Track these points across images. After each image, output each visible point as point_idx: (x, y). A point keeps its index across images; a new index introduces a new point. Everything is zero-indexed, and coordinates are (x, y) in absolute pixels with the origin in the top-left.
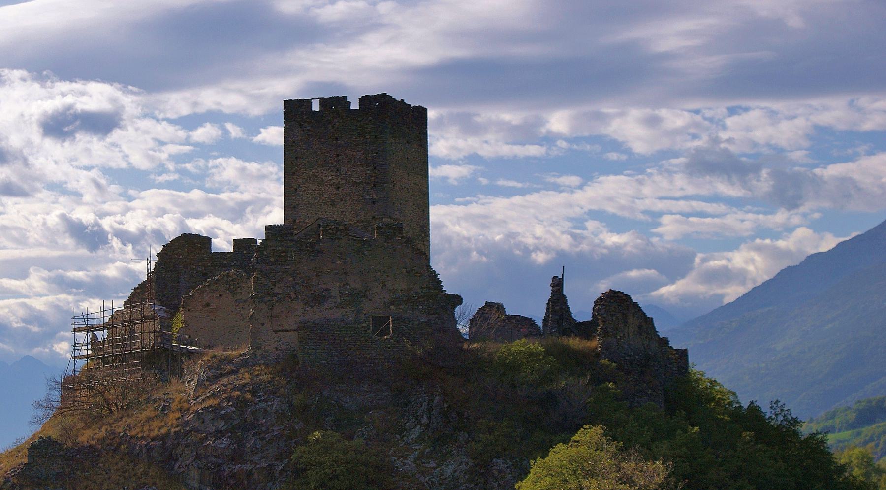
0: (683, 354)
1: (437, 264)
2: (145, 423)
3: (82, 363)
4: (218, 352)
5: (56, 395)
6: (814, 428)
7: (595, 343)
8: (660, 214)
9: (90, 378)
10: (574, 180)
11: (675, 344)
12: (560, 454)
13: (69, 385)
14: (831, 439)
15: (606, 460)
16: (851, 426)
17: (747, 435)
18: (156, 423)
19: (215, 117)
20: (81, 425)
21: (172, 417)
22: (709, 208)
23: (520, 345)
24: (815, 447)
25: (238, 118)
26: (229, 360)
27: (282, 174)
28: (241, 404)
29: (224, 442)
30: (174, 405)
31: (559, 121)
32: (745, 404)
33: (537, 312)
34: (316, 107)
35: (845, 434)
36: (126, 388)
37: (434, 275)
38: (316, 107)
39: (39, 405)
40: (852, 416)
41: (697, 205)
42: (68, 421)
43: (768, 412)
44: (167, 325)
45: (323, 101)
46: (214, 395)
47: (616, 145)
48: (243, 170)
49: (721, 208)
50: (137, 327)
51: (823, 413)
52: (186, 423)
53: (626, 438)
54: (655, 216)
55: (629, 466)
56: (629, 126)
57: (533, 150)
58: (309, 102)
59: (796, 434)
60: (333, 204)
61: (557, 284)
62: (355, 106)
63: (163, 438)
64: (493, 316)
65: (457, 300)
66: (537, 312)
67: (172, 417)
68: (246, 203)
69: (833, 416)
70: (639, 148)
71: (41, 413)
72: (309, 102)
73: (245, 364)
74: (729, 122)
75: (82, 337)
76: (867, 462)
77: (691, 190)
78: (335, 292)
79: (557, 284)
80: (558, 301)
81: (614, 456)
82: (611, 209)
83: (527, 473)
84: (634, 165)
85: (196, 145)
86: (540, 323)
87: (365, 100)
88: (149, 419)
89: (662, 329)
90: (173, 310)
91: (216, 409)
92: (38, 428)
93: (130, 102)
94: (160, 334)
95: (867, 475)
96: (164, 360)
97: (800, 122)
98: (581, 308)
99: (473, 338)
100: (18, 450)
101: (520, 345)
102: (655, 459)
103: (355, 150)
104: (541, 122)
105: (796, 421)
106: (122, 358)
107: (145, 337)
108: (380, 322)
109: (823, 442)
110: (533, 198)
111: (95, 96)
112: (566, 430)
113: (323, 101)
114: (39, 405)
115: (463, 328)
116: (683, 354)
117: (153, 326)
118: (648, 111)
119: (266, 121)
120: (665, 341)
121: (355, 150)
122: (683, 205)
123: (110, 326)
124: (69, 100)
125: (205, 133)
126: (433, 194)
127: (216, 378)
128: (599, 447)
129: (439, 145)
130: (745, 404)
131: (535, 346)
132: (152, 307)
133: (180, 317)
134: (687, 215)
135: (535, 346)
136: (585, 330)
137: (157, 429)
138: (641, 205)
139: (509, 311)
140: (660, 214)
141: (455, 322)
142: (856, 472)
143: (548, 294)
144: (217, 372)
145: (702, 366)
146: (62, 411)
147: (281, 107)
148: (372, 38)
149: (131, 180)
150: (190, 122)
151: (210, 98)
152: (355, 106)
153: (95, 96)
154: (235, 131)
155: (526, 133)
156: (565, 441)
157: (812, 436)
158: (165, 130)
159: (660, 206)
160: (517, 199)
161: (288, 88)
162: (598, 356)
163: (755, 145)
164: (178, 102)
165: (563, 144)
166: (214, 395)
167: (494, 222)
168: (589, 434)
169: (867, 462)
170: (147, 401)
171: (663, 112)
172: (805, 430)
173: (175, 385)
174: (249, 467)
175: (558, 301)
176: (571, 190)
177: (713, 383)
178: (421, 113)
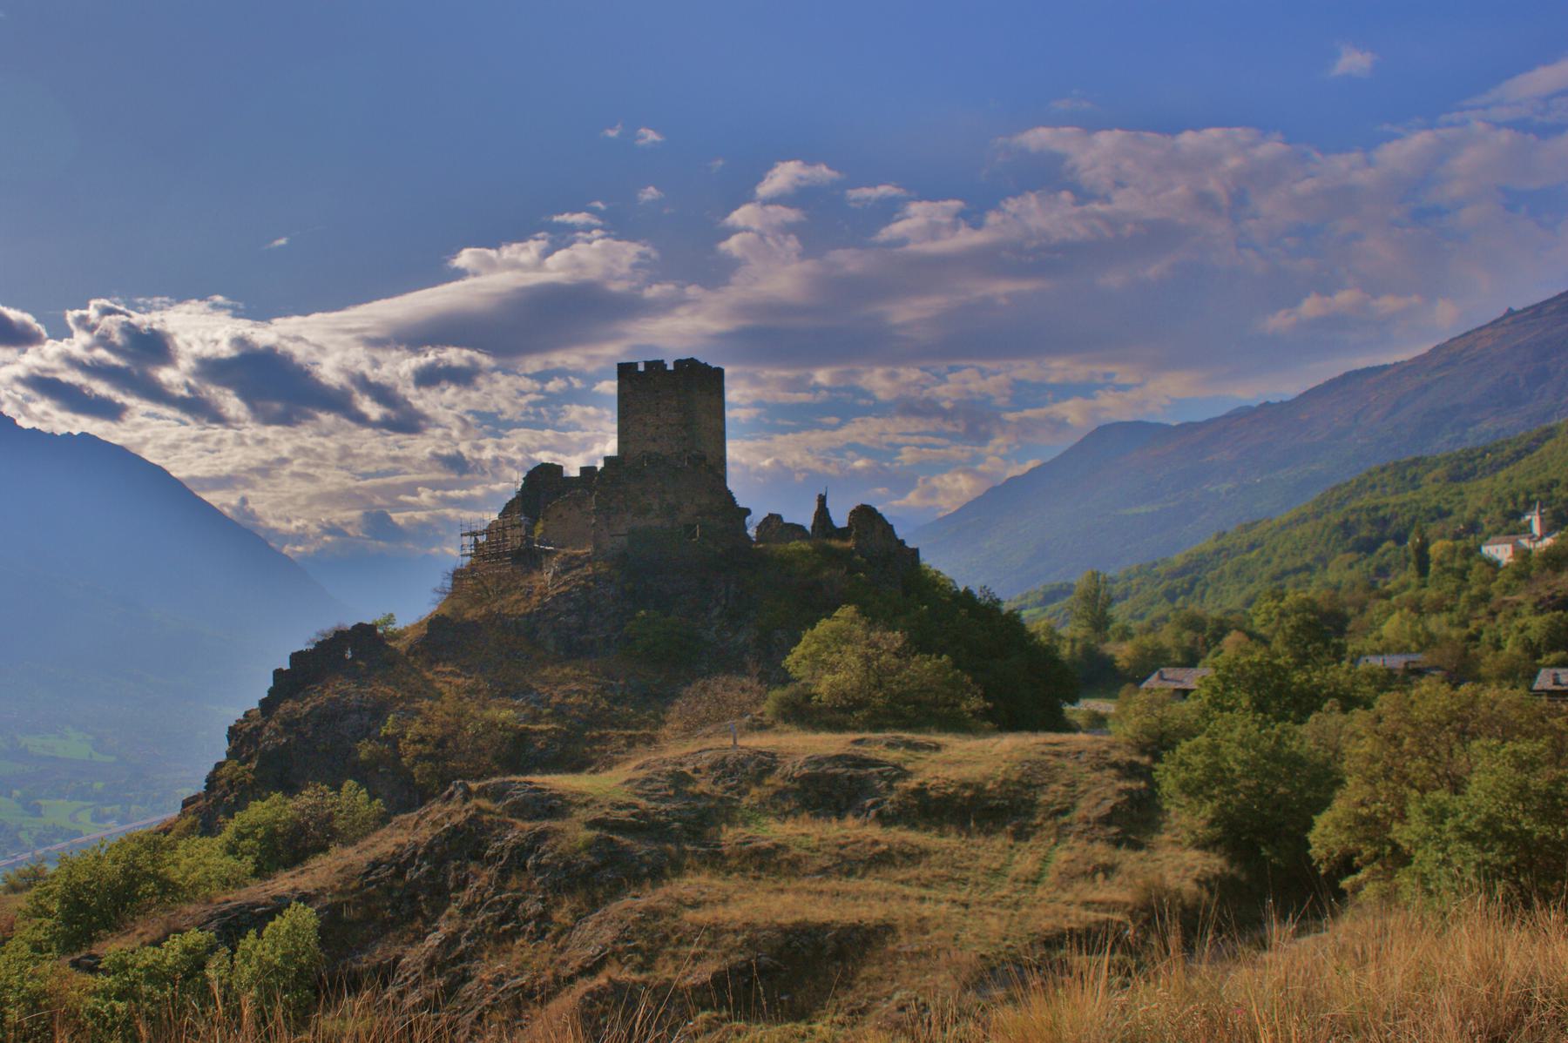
0: (916, 552)
1: (734, 483)
2: (513, 605)
3: (467, 560)
4: (568, 551)
5: (448, 583)
6: (1012, 606)
7: (850, 544)
8: (901, 446)
9: (473, 571)
10: (834, 420)
11: (910, 544)
12: (824, 627)
13: (458, 575)
14: (1025, 614)
15: (859, 631)
16: (1039, 605)
17: (963, 612)
18: (523, 604)
19: (562, 373)
20: (466, 606)
21: (535, 599)
22: (938, 441)
23: (794, 545)
24: (1013, 620)
25: (578, 373)
26: (576, 557)
27: (616, 416)
28: (586, 588)
29: (573, 619)
30: (536, 591)
31: (822, 376)
32: (962, 589)
33: (806, 520)
34: (641, 368)
35: (1035, 611)
36: (500, 578)
37: (729, 493)
38: (641, 368)
39: (435, 591)
40: (1040, 598)
41: (930, 440)
42: (457, 603)
43: (978, 595)
44: (530, 531)
45: (647, 364)
46: (566, 583)
47: (866, 394)
48: (585, 414)
49: (947, 442)
50: (508, 533)
51: (1018, 596)
52: (545, 605)
53: (872, 615)
54: (896, 448)
55: (875, 635)
56: (876, 381)
57: (802, 397)
58: (636, 364)
59: (999, 611)
60: (654, 440)
61: (822, 500)
62: (670, 367)
63: (529, 615)
64: (774, 524)
65: (747, 512)
66: (806, 520)
67: (535, 599)
68: (592, 441)
69: (1026, 597)
70: (881, 395)
71: (437, 596)
72: (636, 364)
73: (589, 560)
74: (950, 377)
75: (468, 540)
76: (1051, 631)
77: (922, 428)
78: (656, 507)
79: (822, 500)
80: (822, 514)
81: (864, 628)
82: (862, 441)
83: (799, 640)
84: (881, 410)
85: (549, 394)
86: (809, 529)
87: (678, 363)
88: (517, 601)
89: (900, 533)
90: (535, 520)
91: (567, 594)
92: (434, 608)
93: (485, 361)
94: (524, 538)
95: (1051, 640)
96: (528, 558)
97: (1002, 377)
98: (840, 518)
99: (759, 540)
100: (421, 624)
101: (794, 545)
102: (894, 630)
103: (672, 402)
104: (811, 376)
105: (999, 601)
106: (498, 556)
107: (514, 540)
108: (690, 529)
109: (1018, 616)
110: (803, 435)
111: (454, 356)
112: (828, 609)
113: (647, 364)
114: (435, 591)
115: (752, 532)
116: (916, 552)
117: (520, 531)
118: (889, 369)
119: (600, 376)
120: (902, 542)
121: (672, 402)
122: (916, 439)
123: (488, 532)
124: (248, 331)
125: (553, 386)
126: (729, 431)
127: (566, 571)
128: (853, 621)
129: (732, 394)
130: (962, 589)
131: (805, 546)
132: (519, 518)
133: (540, 525)
134: (920, 446)
135: (805, 546)
136: (843, 534)
137: (523, 609)
138: (885, 439)
139: (786, 520)
140: (901, 446)
141: (745, 528)
142: (1043, 638)
143: (814, 507)
144: (568, 565)
145: (928, 560)
146: (453, 594)
147: (616, 369)
148: (681, 311)
149: (491, 423)
150: (543, 376)
151: (558, 359)
152: (670, 367)
153: (454, 356)
154: (577, 384)
155: (795, 385)
156: (829, 617)
157: (1011, 612)
158: (526, 384)
159: (900, 440)
160: (791, 436)
161: (613, 352)
162: (853, 553)
163: (969, 392)
164: (533, 363)
165: (824, 393)
166: (566, 583)
167: (768, 465)
168: (846, 611)
169: (1051, 631)
170: (516, 588)
171: (902, 370)
172: (1006, 607)
173: (536, 576)
174: (591, 637)
175: (822, 514)
176: (834, 428)
177: (938, 573)
178: (720, 372)
